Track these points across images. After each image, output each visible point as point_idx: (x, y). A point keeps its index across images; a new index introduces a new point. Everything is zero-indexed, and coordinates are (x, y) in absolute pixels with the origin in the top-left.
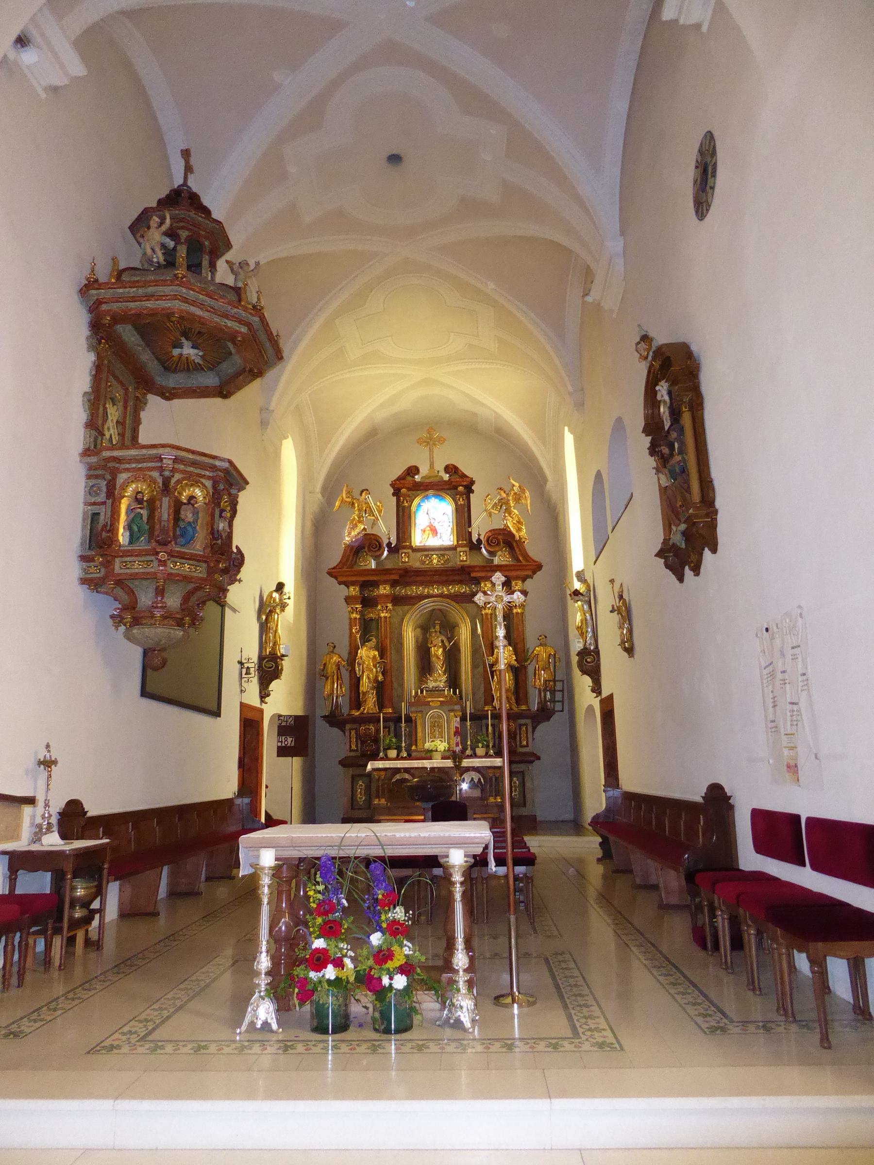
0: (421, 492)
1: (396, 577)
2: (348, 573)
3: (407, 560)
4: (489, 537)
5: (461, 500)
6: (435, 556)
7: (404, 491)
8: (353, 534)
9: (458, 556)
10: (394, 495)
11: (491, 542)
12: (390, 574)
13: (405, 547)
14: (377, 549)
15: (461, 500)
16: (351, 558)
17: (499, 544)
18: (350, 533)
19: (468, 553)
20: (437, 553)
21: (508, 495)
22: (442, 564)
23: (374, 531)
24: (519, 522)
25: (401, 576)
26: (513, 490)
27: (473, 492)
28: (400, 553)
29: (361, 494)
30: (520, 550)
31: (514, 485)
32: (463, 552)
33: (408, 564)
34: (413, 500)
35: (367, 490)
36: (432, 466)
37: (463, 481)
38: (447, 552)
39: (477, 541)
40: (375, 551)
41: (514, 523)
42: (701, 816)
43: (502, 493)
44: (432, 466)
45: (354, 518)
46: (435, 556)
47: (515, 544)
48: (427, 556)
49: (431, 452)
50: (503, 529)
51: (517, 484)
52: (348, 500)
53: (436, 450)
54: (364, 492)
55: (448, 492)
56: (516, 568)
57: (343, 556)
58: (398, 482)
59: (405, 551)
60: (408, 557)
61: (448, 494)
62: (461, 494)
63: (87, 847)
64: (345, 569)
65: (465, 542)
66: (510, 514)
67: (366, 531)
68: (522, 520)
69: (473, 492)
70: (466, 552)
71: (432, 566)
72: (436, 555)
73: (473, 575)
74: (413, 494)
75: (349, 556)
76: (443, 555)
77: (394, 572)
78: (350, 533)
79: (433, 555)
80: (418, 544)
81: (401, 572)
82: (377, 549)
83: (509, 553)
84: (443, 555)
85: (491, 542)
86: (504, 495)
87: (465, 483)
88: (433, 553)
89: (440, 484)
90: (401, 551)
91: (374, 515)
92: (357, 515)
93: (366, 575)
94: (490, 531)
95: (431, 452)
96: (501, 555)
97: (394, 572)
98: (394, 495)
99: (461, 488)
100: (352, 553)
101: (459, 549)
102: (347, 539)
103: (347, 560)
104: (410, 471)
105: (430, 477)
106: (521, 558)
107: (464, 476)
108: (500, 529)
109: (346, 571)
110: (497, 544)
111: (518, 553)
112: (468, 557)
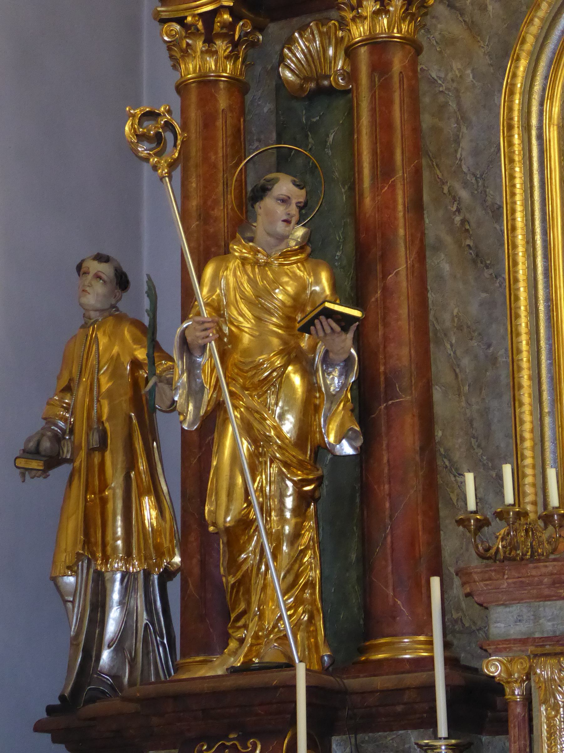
42: (470, 478)
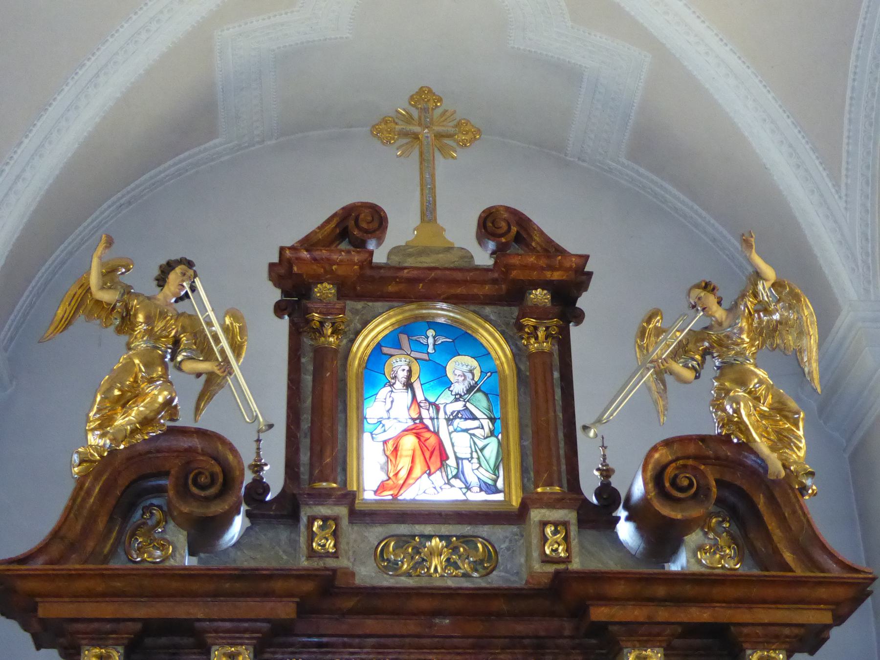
0: (387, 304)
1: (285, 610)
2: (81, 585)
3: (330, 544)
4: (664, 468)
5: (541, 334)
6: (435, 542)
7: (325, 290)
8: (120, 421)
9: (535, 541)
10: (279, 309)
11: (674, 483)
12: (268, 595)
13: (323, 497)
14: (212, 491)
15: (541, 334)
16: (101, 525)
17: (700, 495)
18: (106, 422)
19: (574, 530)
20: (445, 530)
21: (733, 309)
22: (465, 575)
23: (208, 421)
24: (780, 409)
25: (305, 609)
26: (755, 295)
27: (579, 317)
28: (304, 519)
29: (161, 281)
30: (782, 520)
31: (758, 275)
32: (556, 524)
33: (331, 563)
34: (357, 333)
35: (190, 264)
36: (428, 213)
37: (552, 268)
38: (484, 530)
39: (598, 493)
40: (208, 500)
41: (763, 415)
43: (712, 300)
44: (428, 213)
45: (130, 364)
46: (435, 542)
47: (761, 502)
48: (403, 541)
49: (426, 165)
50: (725, 440)
51: (770, 273)
52: (107, 296)
53: (441, 165)
54: (179, 270)
55: (487, 310)
56: (770, 592)
57: (69, 510)
58: (305, 254)
59: (324, 510)
60: (335, 534)
61: (487, 319)
62: (541, 314)
63: (222, 331)
64: (73, 565)
65: (557, 489)
66: (742, 381)
67: (173, 416)
68: (793, 404)
69: (579, 317)
70: (565, 524)
71: (424, 582)
72: (441, 537)
73: (599, 613)
74: (355, 312)
75: (92, 517)
76: (468, 540)
77: (278, 585)
78: (106, 422)
79: (430, 537)
80: (369, 495)
81: (308, 587)
82: (212, 491)
83: (733, 539)
84: (468, 540)
85: (674, 483)
86: (719, 313)
87: (556, 276)
88: (428, 529)
89: (459, 276)
90: (305, 513)
91: (209, 355)
92: (140, 355)
93: (157, 595)
94: (668, 443)
95: (426, 165)
96: (701, 548)
97: (278, 585)
98: (279, 309)
99: (539, 296)
100: (111, 501)
101: (536, 515)
102: (93, 439)
103: (86, 532)
104: (351, 223)
105: (425, 251)
106: (788, 557)
107: (552, 250)
108: (703, 439)
109: (80, 576)
110: (695, 495)
111: (777, 533)
112: (574, 543)
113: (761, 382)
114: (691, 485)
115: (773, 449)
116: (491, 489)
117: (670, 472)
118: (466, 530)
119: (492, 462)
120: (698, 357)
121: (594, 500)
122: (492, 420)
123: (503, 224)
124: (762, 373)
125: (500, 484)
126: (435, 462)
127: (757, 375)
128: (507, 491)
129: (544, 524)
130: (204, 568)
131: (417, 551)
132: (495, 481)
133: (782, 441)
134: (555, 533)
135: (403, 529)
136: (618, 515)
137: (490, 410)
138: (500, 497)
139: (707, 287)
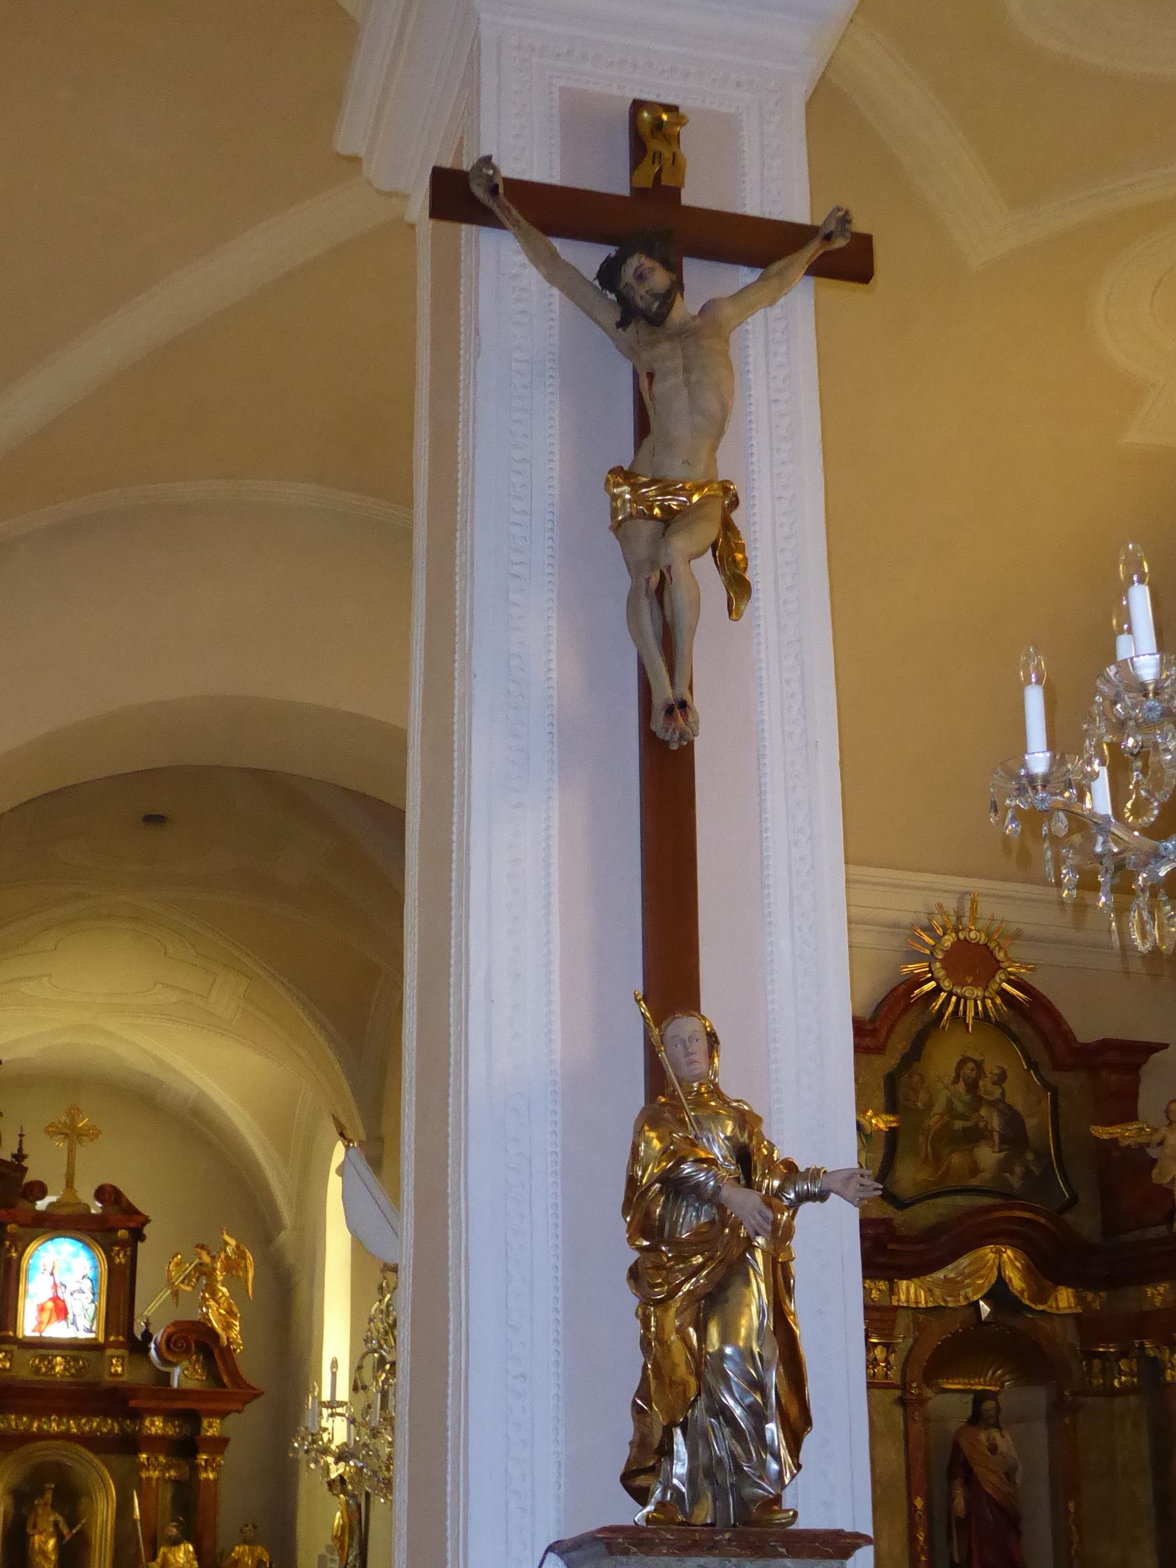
5: (121, 1255)
15: (121, 1255)
20: (64, 1353)
26: (225, 1252)
31: (227, 1243)
38: (85, 1354)
73: (132, 1403)
88: (56, 1352)
96: (187, 1369)
113: (224, 1295)
114: (183, 1346)
115: (224, 1329)
116: (91, 1331)
117: (173, 1339)
118: (75, 1353)
119: (92, 1316)
120: (194, 1280)
121: (139, 1337)
122: (94, 1294)
123: (107, 1196)
124: (224, 1290)
125: (94, 1328)
126: (62, 1314)
127: (221, 1291)
128: (97, 1333)
129: (112, 1357)
130: (641, 388)
131: (50, 1362)
132: (91, 1327)
133: (228, 1327)
134: (117, 1361)
135: (43, 1352)
136: (629, 329)
137: (93, 1289)
138: (92, 1335)
139: (202, 1247)
